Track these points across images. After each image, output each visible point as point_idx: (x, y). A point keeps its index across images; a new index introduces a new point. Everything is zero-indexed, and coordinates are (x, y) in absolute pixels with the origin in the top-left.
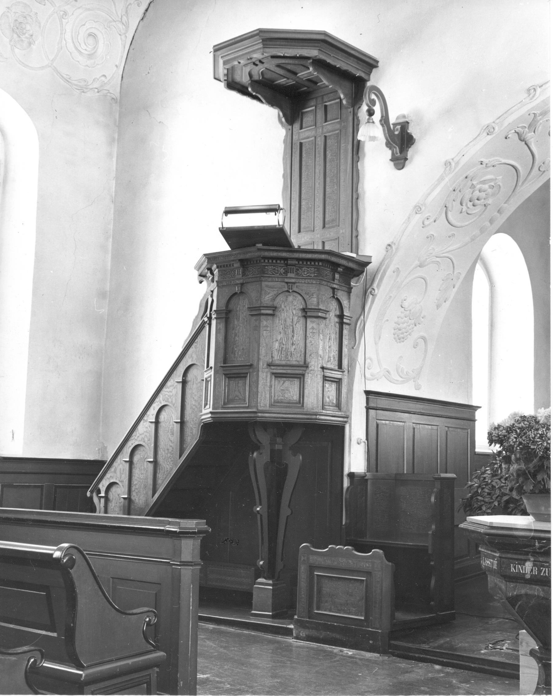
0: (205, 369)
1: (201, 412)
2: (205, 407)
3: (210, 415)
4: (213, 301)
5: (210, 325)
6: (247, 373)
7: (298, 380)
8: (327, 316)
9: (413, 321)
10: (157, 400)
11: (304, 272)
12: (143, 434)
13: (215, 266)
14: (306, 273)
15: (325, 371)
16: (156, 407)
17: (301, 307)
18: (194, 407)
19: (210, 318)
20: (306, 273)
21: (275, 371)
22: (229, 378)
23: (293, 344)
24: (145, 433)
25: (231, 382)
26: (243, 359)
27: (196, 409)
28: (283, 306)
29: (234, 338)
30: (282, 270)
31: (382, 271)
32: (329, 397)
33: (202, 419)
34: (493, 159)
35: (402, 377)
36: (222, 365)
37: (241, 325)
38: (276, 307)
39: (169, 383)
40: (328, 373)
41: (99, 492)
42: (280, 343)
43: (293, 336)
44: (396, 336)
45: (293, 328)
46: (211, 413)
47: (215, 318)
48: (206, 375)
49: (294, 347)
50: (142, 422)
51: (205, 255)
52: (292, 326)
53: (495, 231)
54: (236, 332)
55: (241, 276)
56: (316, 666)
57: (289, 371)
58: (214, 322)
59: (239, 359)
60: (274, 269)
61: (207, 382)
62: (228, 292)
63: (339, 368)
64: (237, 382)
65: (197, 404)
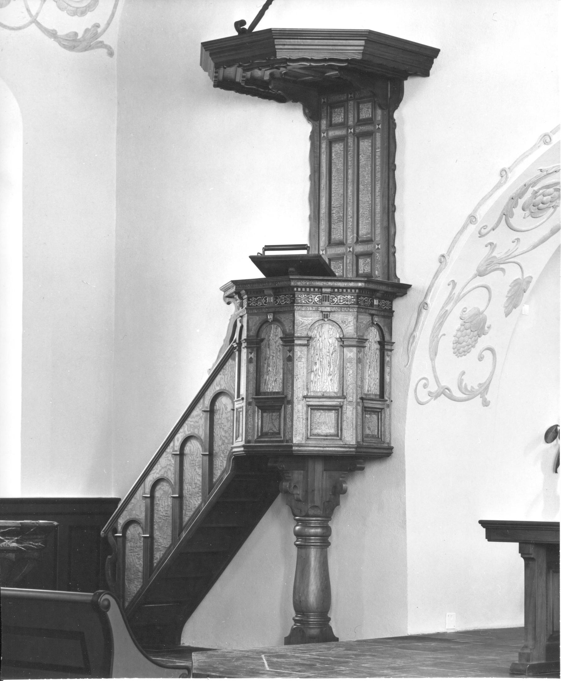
0: (236, 399)
1: (233, 444)
2: (236, 439)
3: (242, 449)
4: (242, 327)
5: (240, 352)
8: (365, 345)
9: (476, 332)
10: (181, 430)
12: (166, 467)
13: (243, 292)
14: (342, 301)
15: (365, 401)
16: (180, 437)
17: (338, 337)
18: (224, 439)
19: (240, 344)
20: (342, 301)
21: (311, 403)
24: (168, 467)
27: (226, 441)
28: (318, 336)
32: (369, 429)
33: (234, 452)
34: (552, 166)
35: (465, 394)
38: (311, 338)
39: (194, 413)
40: (369, 404)
41: (115, 531)
44: (456, 350)
46: (243, 446)
47: (246, 347)
48: (237, 406)
50: (165, 453)
56: (160, 470)
58: (244, 352)
61: (238, 412)
62: (257, 319)
63: (380, 398)
65: (227, 435)
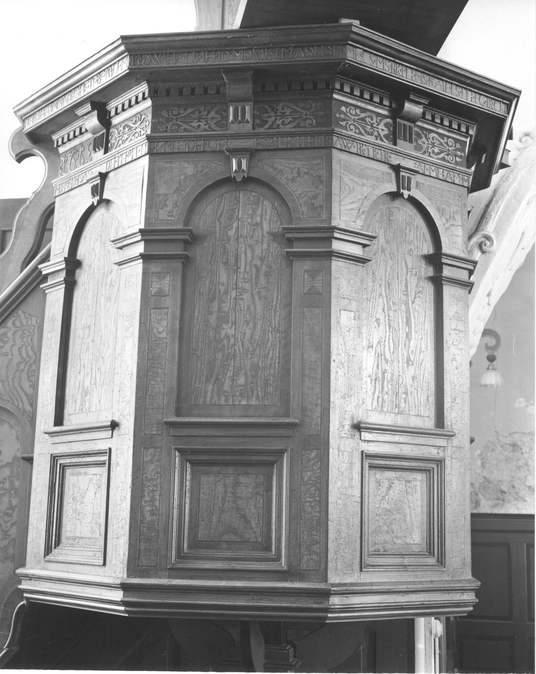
3: (118, 595)
6: (280, 453)
7: (68, 471)
11: (433, 145)
20: (436, 150)
21: (372, 449)
22: (193, 463)
23: (409, 362)
25: (204, 479)
26: (254, 402)
29: (218, 328)
30: (382, 126)
31: (508, 196)
36: (174, 419)
37: (247, 286)
42: (380, 356)
43: (408, 336)
45: (408, 311)
49: (412, 369)
51: (124, 38)
52: (406, 304)
53: (19, 271)
54: (226, 307)
55: (248, 128)
57: (406, 451)
59: (232, 399)
60: (363, 119)
64: (230, 480)
